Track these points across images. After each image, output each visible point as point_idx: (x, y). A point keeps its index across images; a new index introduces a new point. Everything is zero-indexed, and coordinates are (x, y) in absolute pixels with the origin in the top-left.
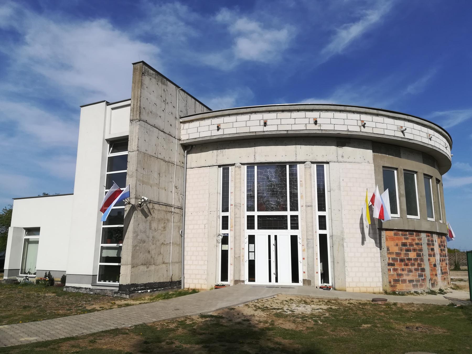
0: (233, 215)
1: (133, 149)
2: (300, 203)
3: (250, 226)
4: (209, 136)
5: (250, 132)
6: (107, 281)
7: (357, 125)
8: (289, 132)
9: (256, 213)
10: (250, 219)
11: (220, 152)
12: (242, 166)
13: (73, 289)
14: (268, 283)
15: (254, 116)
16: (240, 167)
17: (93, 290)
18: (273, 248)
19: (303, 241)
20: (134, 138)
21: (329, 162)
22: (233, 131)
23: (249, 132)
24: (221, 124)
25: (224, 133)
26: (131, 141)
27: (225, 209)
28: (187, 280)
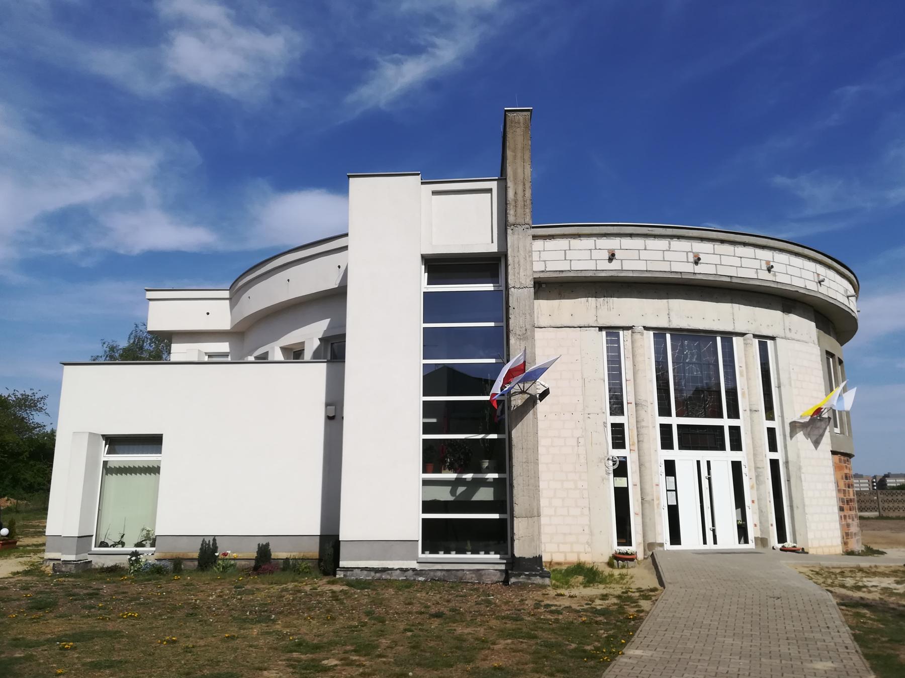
0: (633, 421)
1: (521, 283)
2: (742, 405)
3: (667, 444)
4: (591, 270)
5: (671, 272)
6: (440, 552)
8: (734, 280)
9: (674, 421)
10: (666, 430)
11: (602, 302)
12: (645, 332)
13: (365, 572)
14: (702, 547)
15: (676, 244)
16: (642, 334)
17: (424, 572)
18: (705, 483)
19: (750, 470)
20: (522, 261)
21: (775, 337)
22: (641, 266)
23: (669, 272)
25: (622, 268)
26: (516, 267)
27: (617, 407)
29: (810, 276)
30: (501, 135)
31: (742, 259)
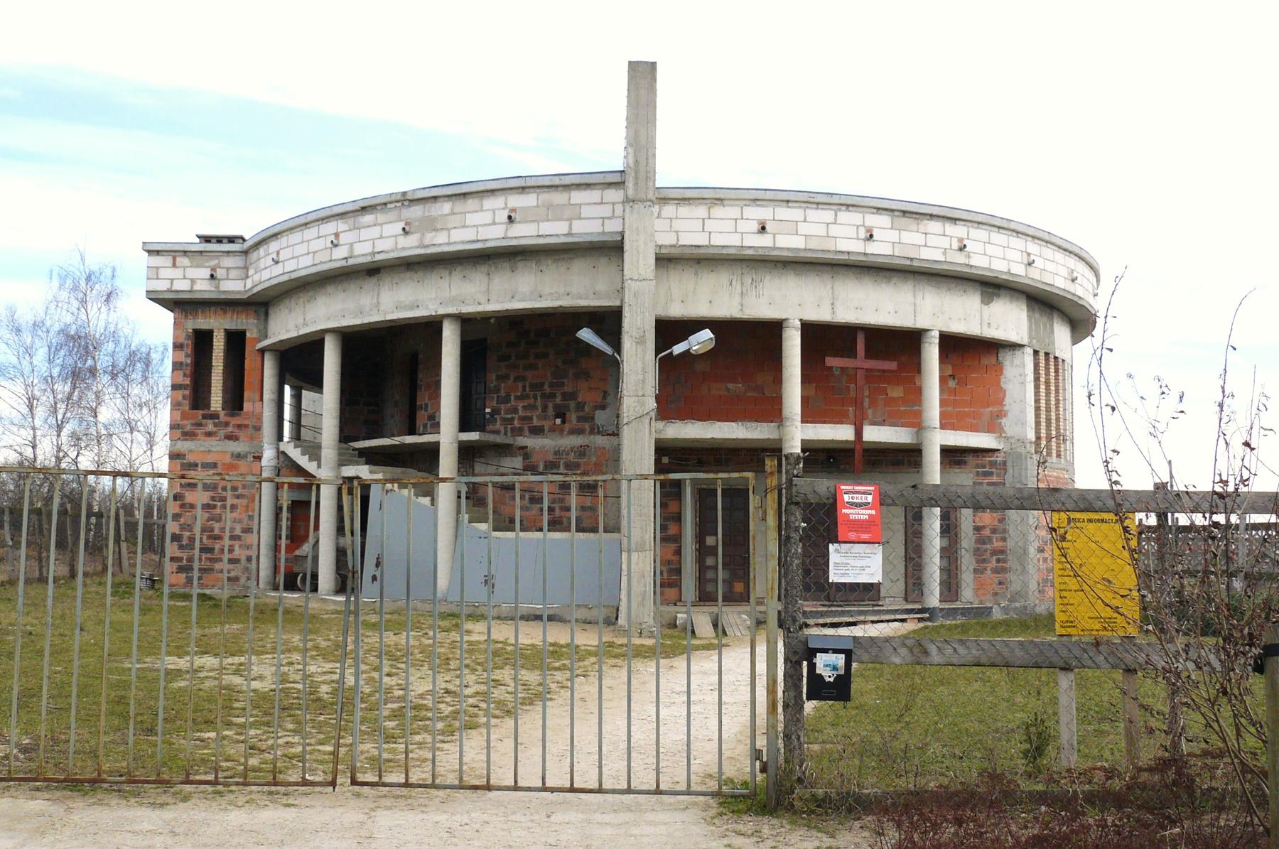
7: (1022, 263)
24: (198, 281)
28: (571, 225)
29: (1016, 256)
30: (589, 175)
31: (928, 236)
